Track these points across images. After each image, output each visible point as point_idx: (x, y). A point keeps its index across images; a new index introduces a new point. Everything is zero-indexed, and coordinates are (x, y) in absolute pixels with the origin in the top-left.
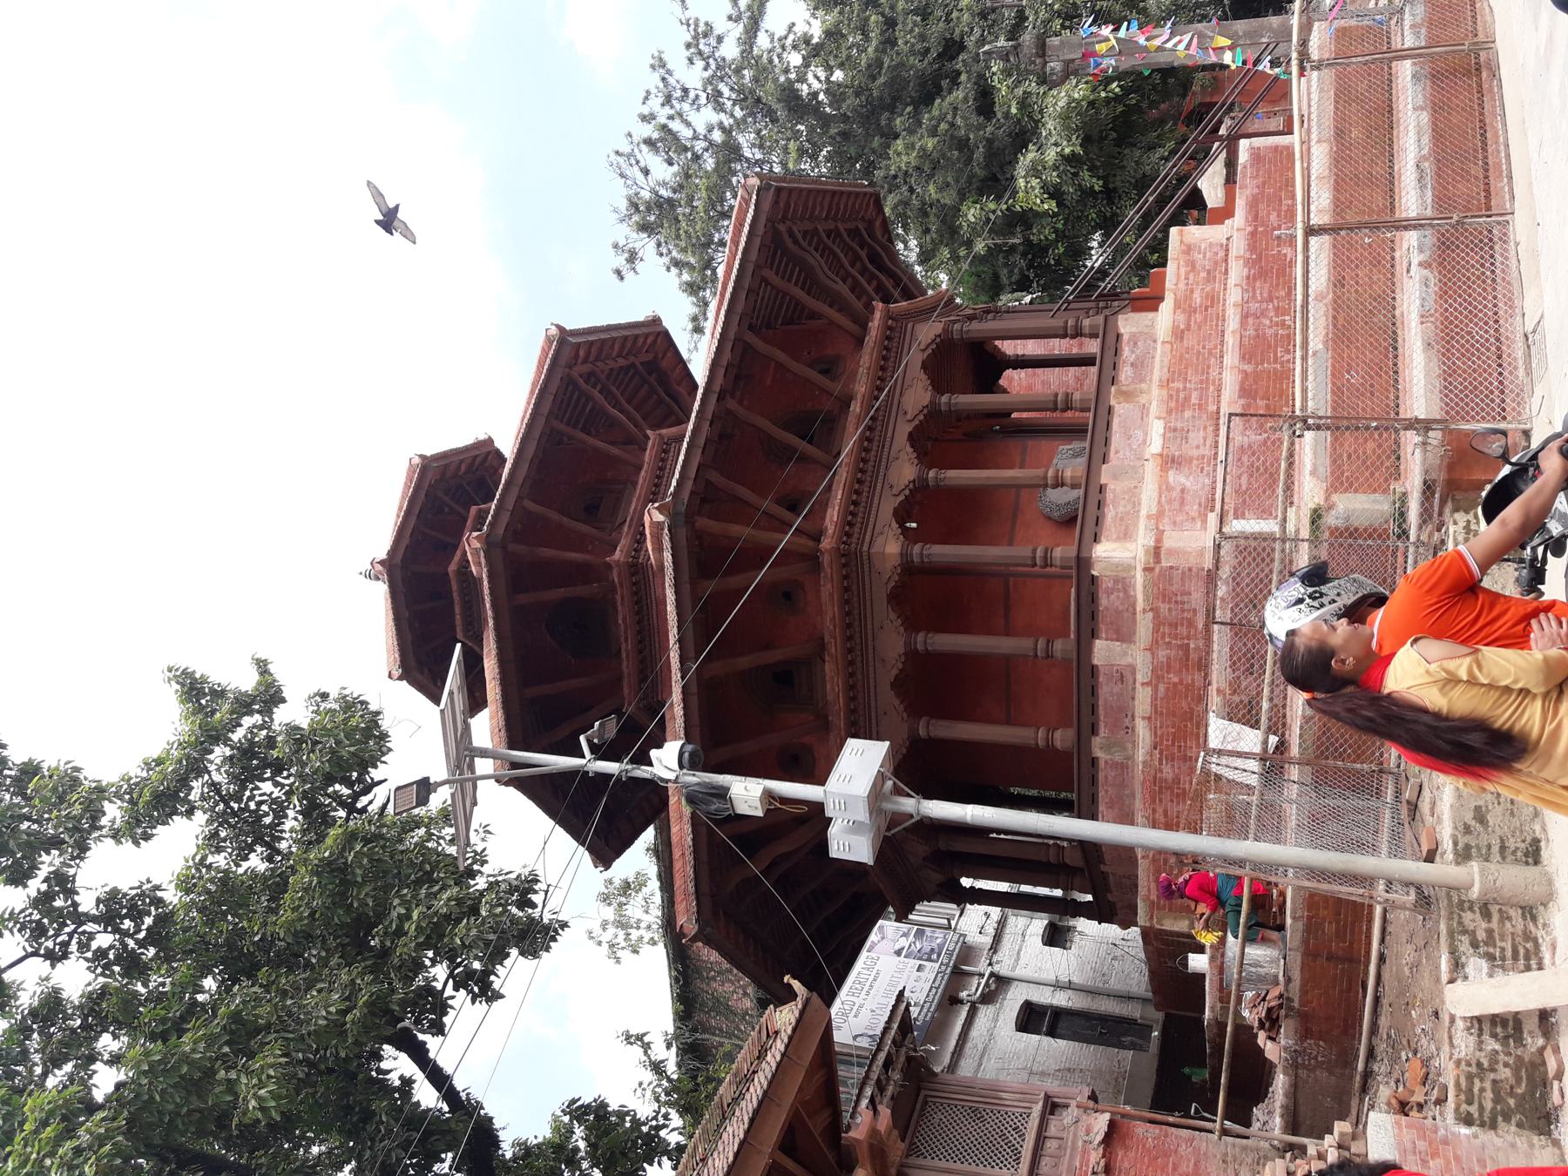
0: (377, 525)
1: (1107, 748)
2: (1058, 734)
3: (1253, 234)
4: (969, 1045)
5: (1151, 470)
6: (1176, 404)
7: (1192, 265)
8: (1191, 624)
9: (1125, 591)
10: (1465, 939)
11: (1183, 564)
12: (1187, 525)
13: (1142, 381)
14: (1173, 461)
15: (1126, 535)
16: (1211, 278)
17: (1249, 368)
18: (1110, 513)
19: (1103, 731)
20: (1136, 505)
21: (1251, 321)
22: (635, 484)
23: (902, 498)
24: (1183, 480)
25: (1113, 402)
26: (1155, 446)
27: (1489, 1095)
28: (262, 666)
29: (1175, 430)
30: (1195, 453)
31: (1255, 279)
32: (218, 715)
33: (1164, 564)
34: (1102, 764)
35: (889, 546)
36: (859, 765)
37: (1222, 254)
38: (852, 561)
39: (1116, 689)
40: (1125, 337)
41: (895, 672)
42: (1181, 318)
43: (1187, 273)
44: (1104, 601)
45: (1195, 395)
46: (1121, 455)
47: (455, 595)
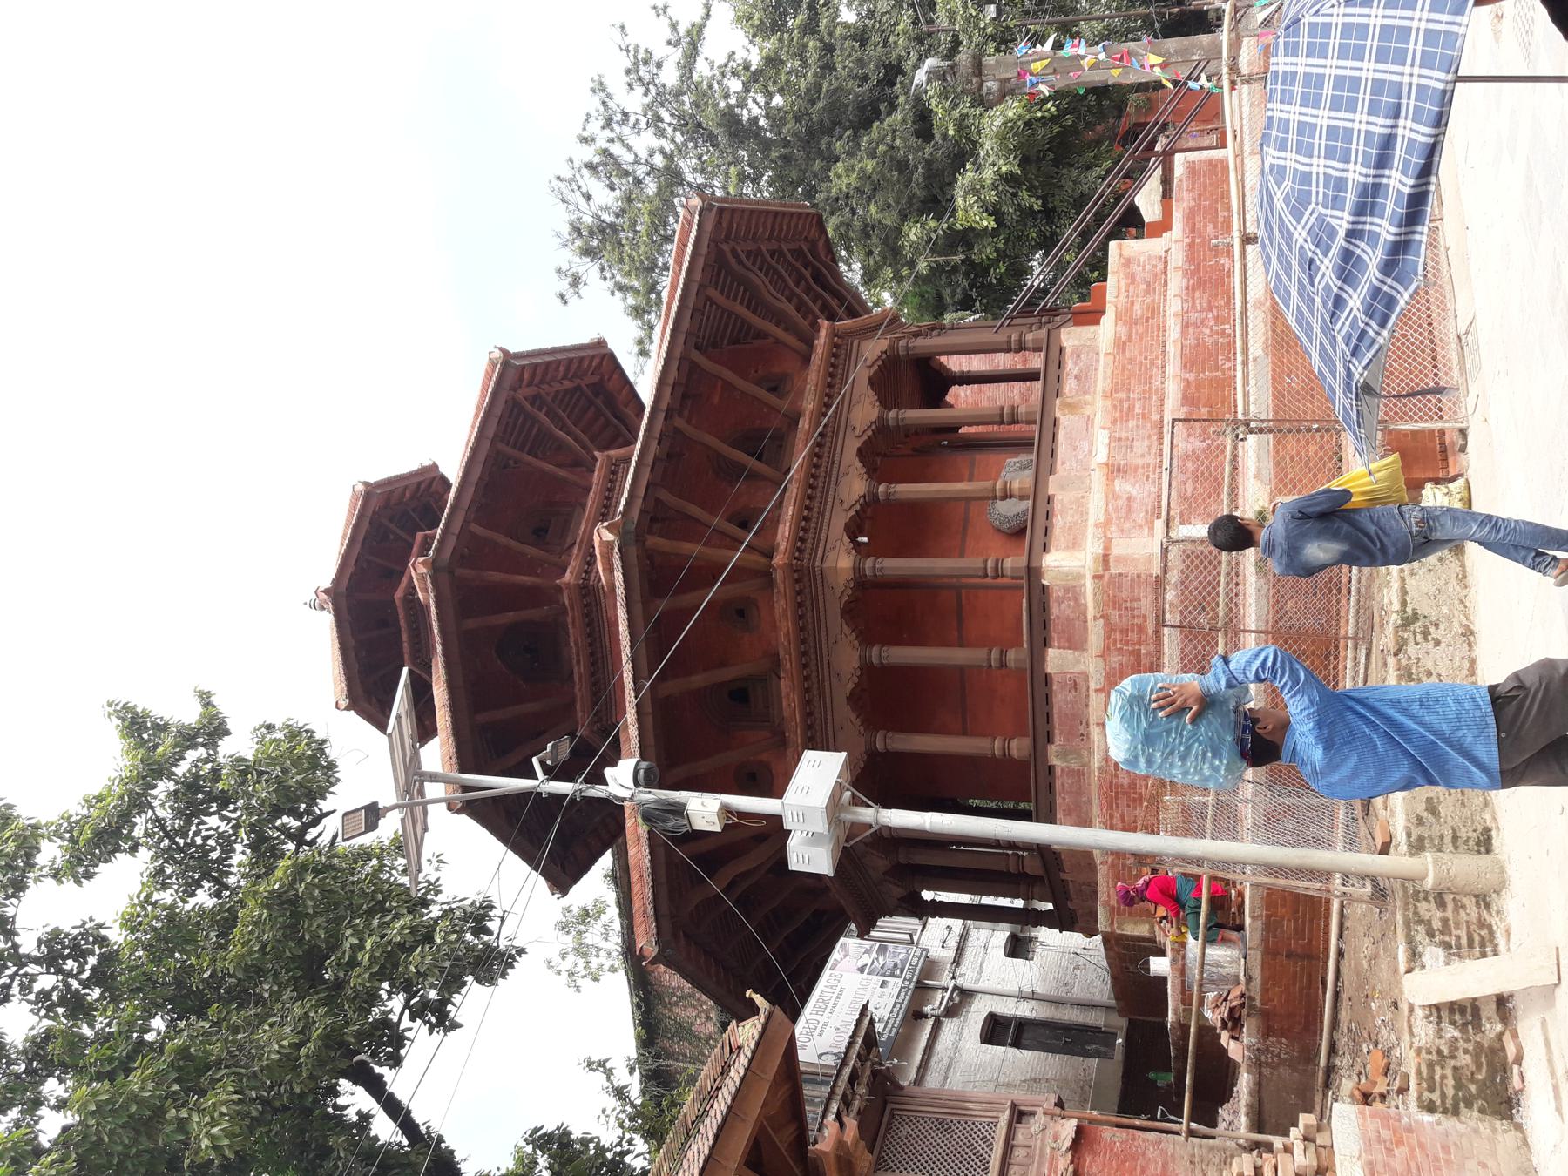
0: (322, 554)
1: (1063, 755)
2: (1014, 743)
3: (1191, 246)
4: (934, 1059)
5: (1097, 479)
6: (1120, 414)
7: (1132, 278)
8: (1141, 629)
9: (1076, 600)
10: (1421, 929)
11: (1132, 570)
12: (1135, 532)
13: (1085, 393)
14: (1119, 470)
15: (1075, 544)
16: (1150, 289)
17: (1191, 376)
18: (1058, 523)
19: (1058, 739)
20: (1084, 514)
21: (1191, 330)
22: (584, 506)
23: (853, 512)
24: (1128, 487)
25: (1058, 414)
26: (1101, 455)
27: (1450, 1082)
28: (205, 699)
29: (1120, 439)
30: (1140, 461)
31: (1194, 290)
32: (161, 749)
33: (1114, 571)
34: (1058, 772)
35: (841, 561)
36: (817, 776)
37: (1160, 266)
38: (806, 576)
39: (1070, 697)
40: (1068, 351)
41: (850, 686)
42: (1123, 330)
43: (1127, 286)
44: (1055, 610)
45: (1138, 405)
46: (1067, 466)
47: (402, 623)
